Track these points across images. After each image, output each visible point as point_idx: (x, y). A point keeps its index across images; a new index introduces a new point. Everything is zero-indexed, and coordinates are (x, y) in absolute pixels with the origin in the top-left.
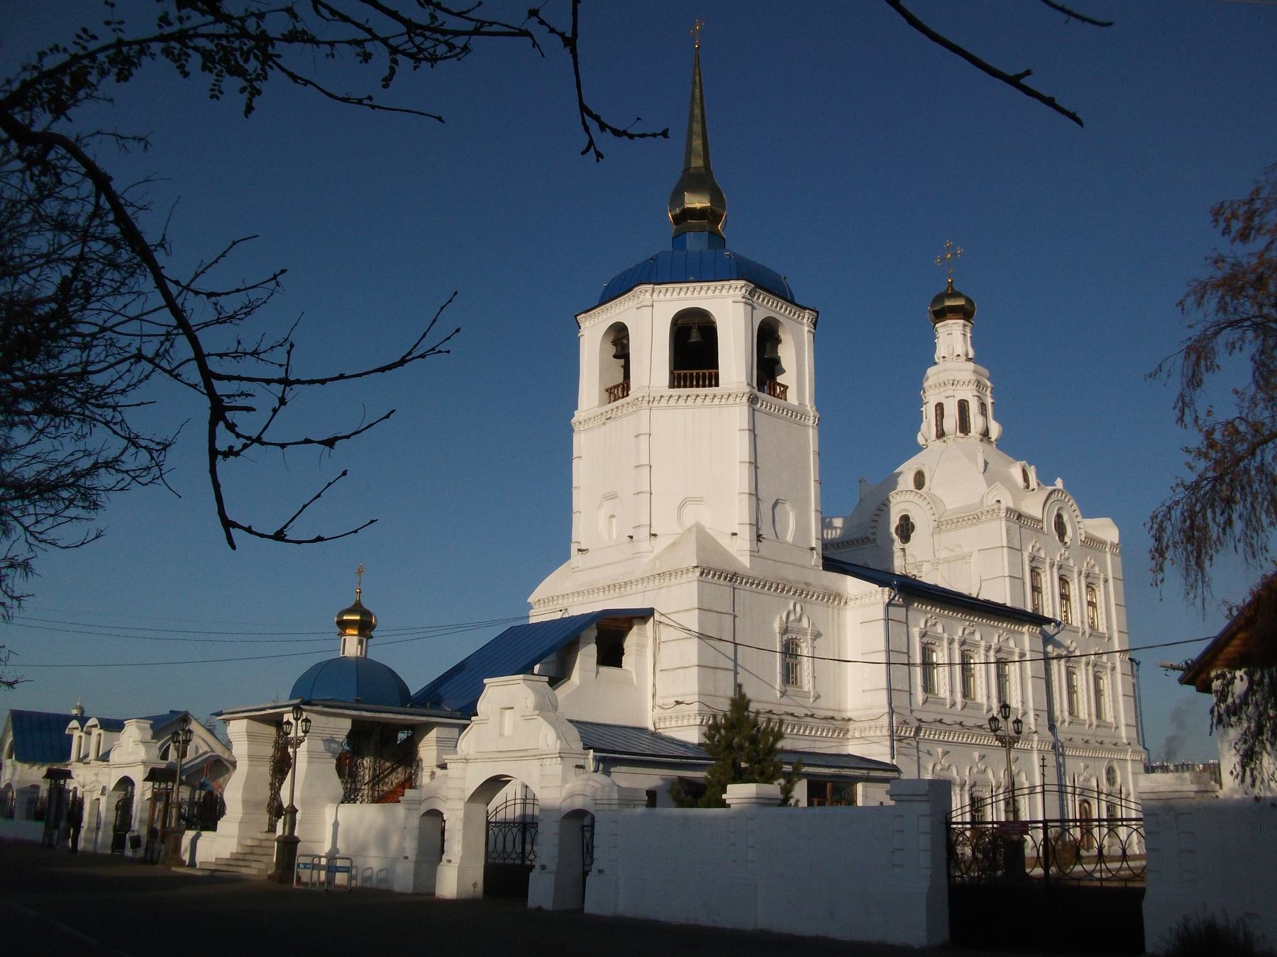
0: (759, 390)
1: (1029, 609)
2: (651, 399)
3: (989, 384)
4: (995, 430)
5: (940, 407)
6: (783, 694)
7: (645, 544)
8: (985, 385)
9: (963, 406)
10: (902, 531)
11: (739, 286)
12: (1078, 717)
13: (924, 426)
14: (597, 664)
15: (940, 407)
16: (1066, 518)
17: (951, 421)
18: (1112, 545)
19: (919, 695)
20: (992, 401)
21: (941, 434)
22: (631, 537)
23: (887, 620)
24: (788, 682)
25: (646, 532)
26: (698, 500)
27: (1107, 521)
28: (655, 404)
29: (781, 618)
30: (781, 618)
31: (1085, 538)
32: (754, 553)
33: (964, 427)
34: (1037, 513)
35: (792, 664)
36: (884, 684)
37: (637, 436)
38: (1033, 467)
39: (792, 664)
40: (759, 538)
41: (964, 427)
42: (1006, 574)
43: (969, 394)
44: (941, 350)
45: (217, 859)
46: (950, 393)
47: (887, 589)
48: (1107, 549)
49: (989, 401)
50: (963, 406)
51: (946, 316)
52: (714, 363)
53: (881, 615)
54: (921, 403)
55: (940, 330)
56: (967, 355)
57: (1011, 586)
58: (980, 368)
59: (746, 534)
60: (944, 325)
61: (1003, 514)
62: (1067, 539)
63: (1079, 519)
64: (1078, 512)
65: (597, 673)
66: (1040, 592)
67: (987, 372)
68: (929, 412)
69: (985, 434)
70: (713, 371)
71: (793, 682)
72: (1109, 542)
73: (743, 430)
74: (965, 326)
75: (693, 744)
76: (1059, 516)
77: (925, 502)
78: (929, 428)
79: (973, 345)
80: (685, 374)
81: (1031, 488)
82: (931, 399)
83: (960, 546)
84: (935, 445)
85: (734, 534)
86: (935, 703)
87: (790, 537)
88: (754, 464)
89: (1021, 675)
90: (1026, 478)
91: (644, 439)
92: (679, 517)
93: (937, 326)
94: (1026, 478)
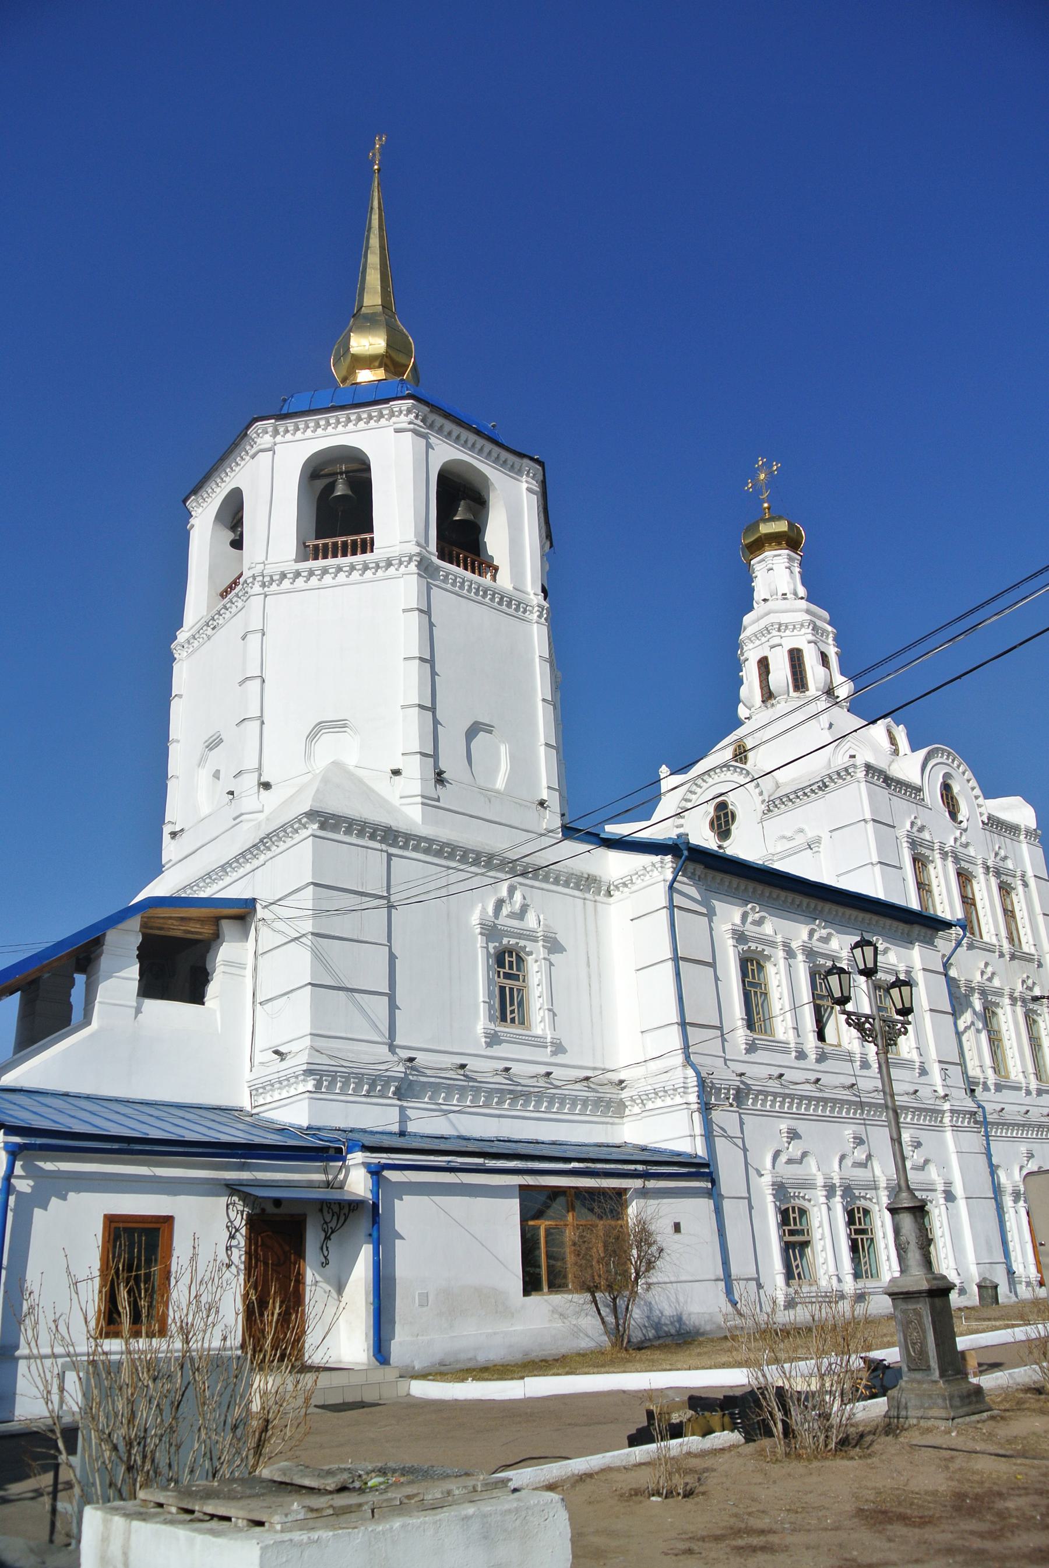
0: (442, 556)
1: (914, 905)
2: (267, 579)
3: (830, 628)
4: (844, 689)
5: (764, 664)
6: (493, 1039)
7: (250, 799)
8: (824, 631)
9: (796, 657)
10: (719, 826)
11: (404, 408)
12: (1007, 1077)
13: (743, 691)
14: (138, 995)
15: (764, 664)
16: (956, 789)
17: (781, 674)
18: (1028, 833)
19: (740, 1035)
20: (836, 649)
21: (768, 695)
22: (231, 793)
23: (671, 907)
24: (503, 1019)
25: (251, 780)
26: (340, 725)
27: (1017, 800)
28: (274, 587)
29: (484, 909)
30: (484, 909)
31: (989, 819)
32: (430, 802)
33: (799, 681)
34: (914, 777)
35: (511, 990)
36: (675, 1017)
37: (244, 638)
38: (901, 726)
39: (511, 990)
40: (440, 778)
41: (799, 681)
42: (875, 860)
43: (801, 640)
44: (761, 588)
45: (724, 1396)
46: (776, 641)
47: (669, 858)
48: (1022, 837)
49: (832, 651)
50: (796, 657)
51: (763, 546)
52: (366, 524)
53: (663, 901)
54: (737, 666)
55: (757, 567)
56: (795, 594)
57: (958, 1158)
58: (814, 608)
59: (414, 770)
60: (763, 560)
61: (861, 774)
62: (960, 818)
63: (981, 800)
64: (977, 791)
65: (138, 1011)
66: (930, 891)
67: (826, 615)
68: (750, 673)
69: (830, 692)
70: (367, 536)
71: (513, 1020)
72: (1023, 827)
73: (411, 610)
74: (791, 559)
75: (300, 1128)
76: (946, 788)
77: (757, 790)
78: (751, 690)
79: (804, 584)
80: (325, 545)
81: (901, 753)
82: (751, 655)
83: (801, 831)
84: (763, 716)
85: (396, 772)
86: (766, 1049)
87: (500, 784)
88: (429, 661)
89: (793, 612)
90: (893, 740)
91: (254, 639)
92: (308, 755)
93: (752, 562)
94: (893, 740)
